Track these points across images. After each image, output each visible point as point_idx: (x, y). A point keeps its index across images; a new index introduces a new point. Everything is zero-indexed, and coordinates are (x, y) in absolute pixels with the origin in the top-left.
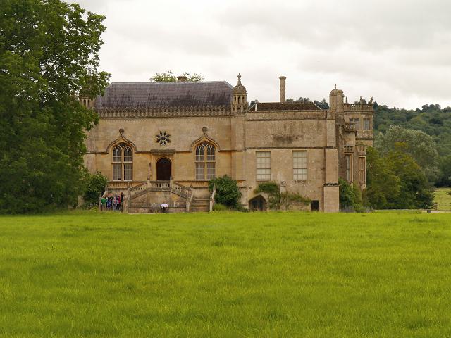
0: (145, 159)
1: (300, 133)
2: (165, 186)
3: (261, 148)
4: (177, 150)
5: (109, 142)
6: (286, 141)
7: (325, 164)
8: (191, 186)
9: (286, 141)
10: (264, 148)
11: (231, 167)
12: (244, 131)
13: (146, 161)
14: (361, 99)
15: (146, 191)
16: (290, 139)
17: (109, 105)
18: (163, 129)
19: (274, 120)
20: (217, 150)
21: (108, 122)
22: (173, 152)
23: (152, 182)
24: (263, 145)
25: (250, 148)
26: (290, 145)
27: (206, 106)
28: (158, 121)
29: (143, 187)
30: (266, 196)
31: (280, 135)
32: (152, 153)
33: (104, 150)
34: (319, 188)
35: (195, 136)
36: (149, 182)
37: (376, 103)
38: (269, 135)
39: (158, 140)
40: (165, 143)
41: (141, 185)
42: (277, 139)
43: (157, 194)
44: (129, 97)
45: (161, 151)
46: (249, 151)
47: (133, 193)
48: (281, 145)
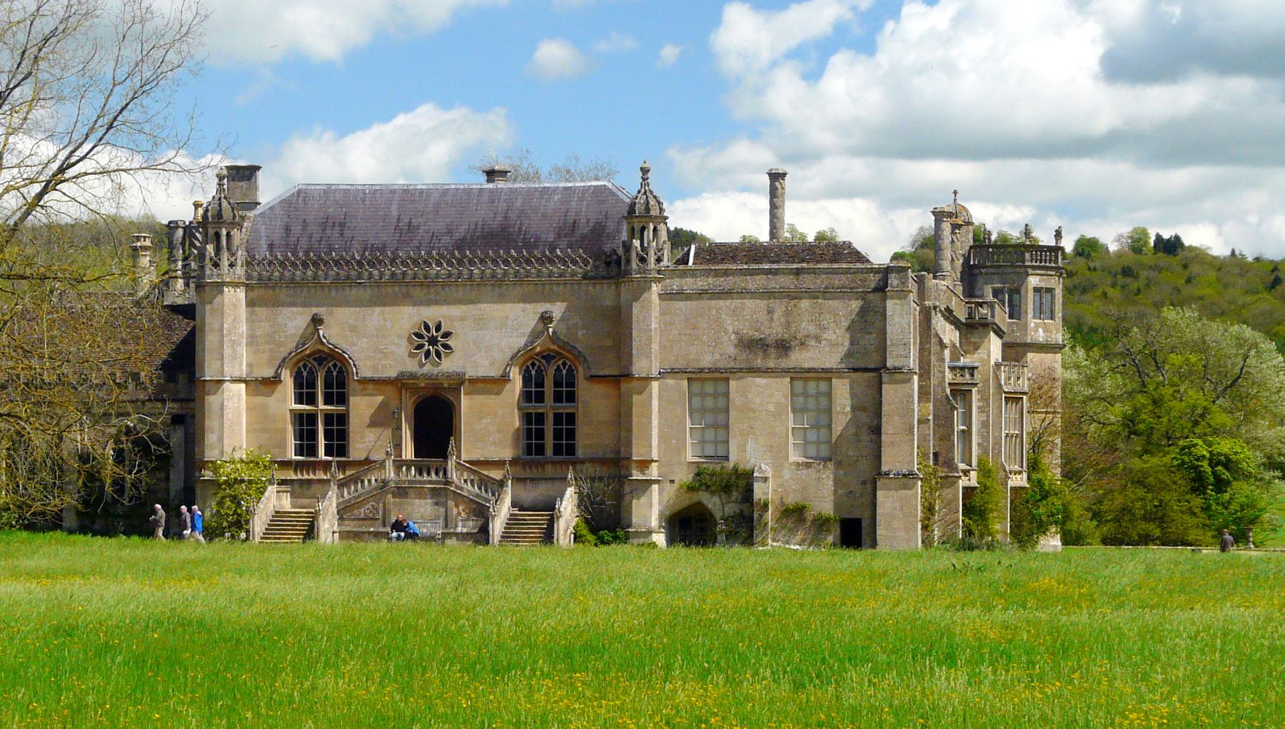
1: (812, 329)
4: (470, 373)
6: (772, 351)
7: (878, 415)
9: (772, 351)
11: (619, 424)
14: (1233, 252)
16: (783, 347)
17: (287, 245)
20: (581, 373)
22: (458, 382)
23: (399, 464)
24: (707, 361)
26: (785, 363)
27: (553, 250)
30: (713, 503)
31: (757, 335)
32: (401, 383)
34: (864, 483)
37: (676, 228)
38: (726, 331)
42: (751, 344)
44: (342, 225)
48: (759, 362)
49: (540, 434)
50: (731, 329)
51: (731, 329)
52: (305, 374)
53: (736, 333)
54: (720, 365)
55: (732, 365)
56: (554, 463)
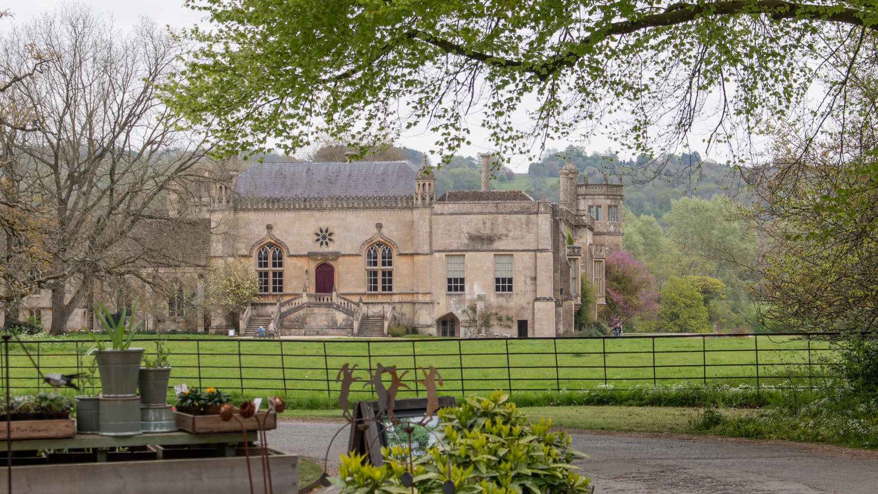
0: (299, 264)
2: (325, 301)
3: (452, 251)
4: (342, 253)
5: (253, 242)
8: (361, 301)
10: (456, 251)
12: (431, 227)
13: (301, 268)
15: (300, 307)
16: (490, 240)
18: (324, 225)
19: (470, 214)
21: (252, 216)
22: (337, 255)
25: (439, 251)
28: (317, 214)
29: (297, 301)
33: (244, 252)
35: (367, 234)
36: (305, 295)
38: (463, 232)
39: (318, 240)
40: (327, 244)
41: (294, 299)
43: (316, 310)
45: (322, 254)
46: (437, 255)
47: (284, 309)
49: (375, 281)
50: (465, 231)
51: (465, 231)
52: (263, 253)
53: (468, 233)
54: (461, 248)
55: (466, 249)
56: (382, 294)
